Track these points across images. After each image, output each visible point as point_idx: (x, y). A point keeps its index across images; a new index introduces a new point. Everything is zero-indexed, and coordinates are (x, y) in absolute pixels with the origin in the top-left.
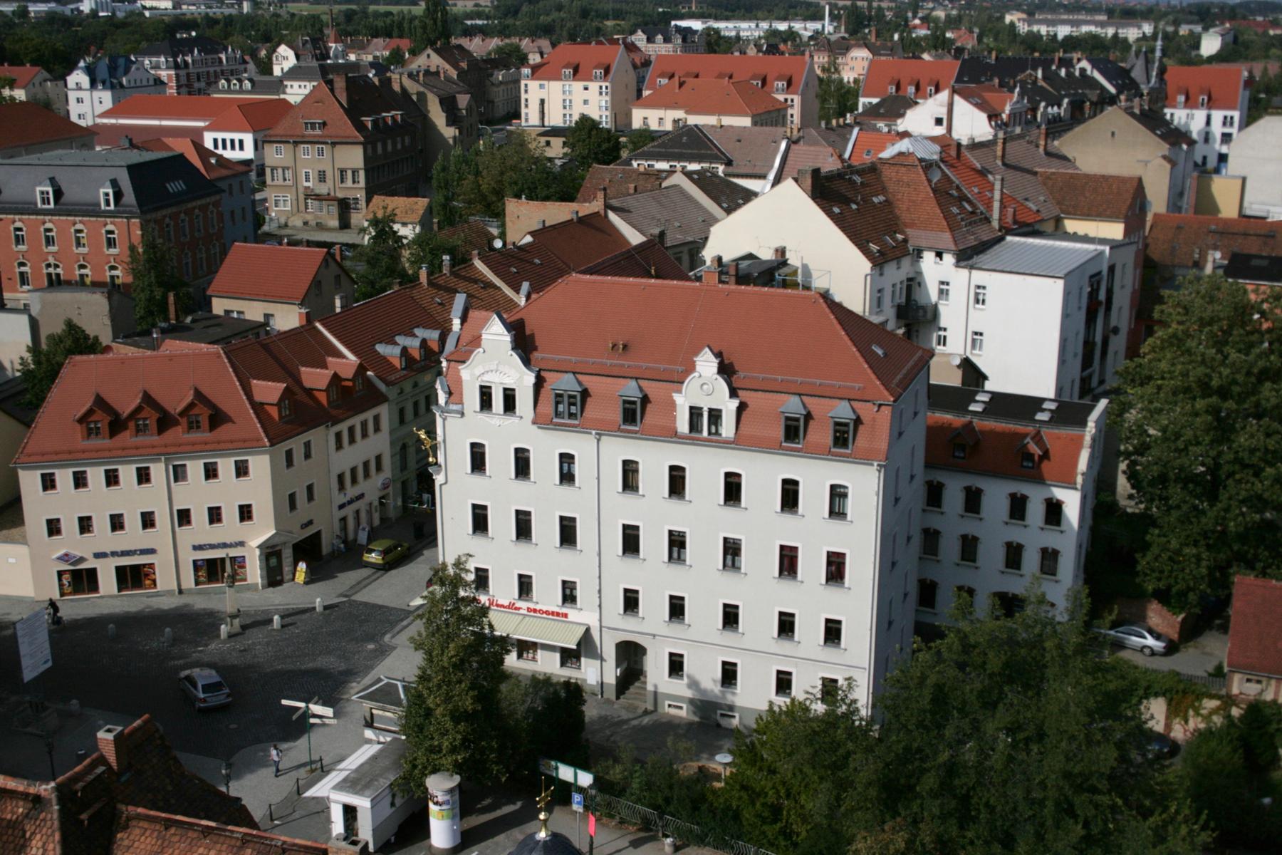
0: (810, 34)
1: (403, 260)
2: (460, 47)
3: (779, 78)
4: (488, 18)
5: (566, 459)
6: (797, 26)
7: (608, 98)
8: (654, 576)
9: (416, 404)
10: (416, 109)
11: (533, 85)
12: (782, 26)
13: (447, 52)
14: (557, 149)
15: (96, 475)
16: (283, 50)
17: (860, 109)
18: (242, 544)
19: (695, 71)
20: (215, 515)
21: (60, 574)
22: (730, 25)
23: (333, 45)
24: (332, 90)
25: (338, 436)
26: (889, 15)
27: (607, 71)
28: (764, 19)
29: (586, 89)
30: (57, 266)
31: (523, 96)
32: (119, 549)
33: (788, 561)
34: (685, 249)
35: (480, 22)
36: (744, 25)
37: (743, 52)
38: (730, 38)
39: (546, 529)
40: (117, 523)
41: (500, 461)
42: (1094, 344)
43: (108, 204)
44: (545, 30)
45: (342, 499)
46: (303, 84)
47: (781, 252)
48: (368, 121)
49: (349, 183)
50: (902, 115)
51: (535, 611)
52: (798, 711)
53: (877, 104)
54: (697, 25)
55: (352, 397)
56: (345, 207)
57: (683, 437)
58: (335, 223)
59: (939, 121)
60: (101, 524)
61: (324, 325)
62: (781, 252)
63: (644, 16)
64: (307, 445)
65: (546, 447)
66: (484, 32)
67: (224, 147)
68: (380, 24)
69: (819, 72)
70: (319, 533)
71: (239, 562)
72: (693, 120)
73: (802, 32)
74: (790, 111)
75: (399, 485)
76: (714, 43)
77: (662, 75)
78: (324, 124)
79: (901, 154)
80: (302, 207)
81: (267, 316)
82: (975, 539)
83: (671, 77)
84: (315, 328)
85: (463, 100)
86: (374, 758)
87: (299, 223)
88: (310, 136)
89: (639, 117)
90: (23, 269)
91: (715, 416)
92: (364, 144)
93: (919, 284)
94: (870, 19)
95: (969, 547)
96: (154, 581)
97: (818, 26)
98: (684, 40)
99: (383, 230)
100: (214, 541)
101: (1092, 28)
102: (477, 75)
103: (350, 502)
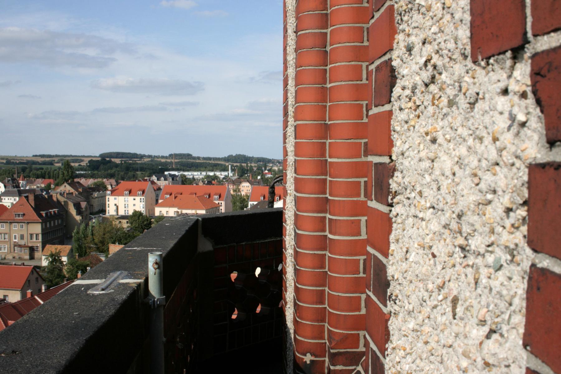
0: (223, 177)
1: (64, 271)
2: (78, 183)
3: (216, 194)
4: (85, 171)
6: (218, 174)
7: (144, 203)
10: (63, 208)
11: (112, 198)
12: (211, 174)
13: (72, 185)
14: (125, 224)
17: (249, 207)
19: (195, 192)
22: (190, 173)
23: (21, 182)
24: (28, 200)
26: (255, 169)
27: (143, 192)
28: (203, 171)
29: (134, 199)
31: (107, 203)
35: (82, 172)
36: (195, 173)
37: (197, 184)
38: (190, 179)
44: (111, 176)
46: (10, 198)
48: (43, 213)
49: (34, 240)
53: (256, 204)
54: (176, 173)
56: (32, 250)
58: (27, 257)
61: (39, 297)
63: (153, 170)
66: (85, 176)
68: (39, 172)
69: (232, 192)
72: (184, 211)
73: (220, 176)
74: (221, 208)
76: (185, 181)
77: (167, 194)
78: (24, 215)
80: (12, 250)
81: (5, 296)
83: (171, 194)
84: (35, 298)
85: (84, 205)
87: (11, 257)
88: (17, 220)
89: (158, 211)
92: (42, 223)
94: (247, 171)
97: (226, 173)
98: (173, 179)
99: (55, 258)
102: (87, 192)
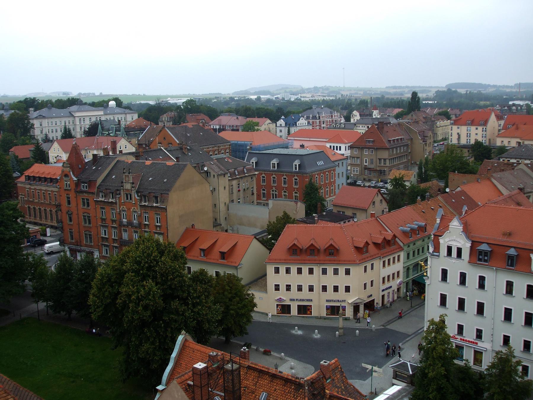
5: (482, 279)
9: (414, 252)
15: (294, 269)
16: (355, 113)
18: (344, 301)
20: (336, 289)
25: (384, 262)
29: (477, 129)
30: (276, 191)
32: (299, 298)
39: (471, 307)
40: (300, 288)
41: (454, 277)
51: (464, 340)
55: (386, 246)
60: (294, 288)
64: (372, 265)
65: (473, 274)
70: (374, 300)
71: (344, 308)
75: (405, 284)
86: (399, 391)
96: (311, 312)
100: (334, 299)
103: (386, 289)
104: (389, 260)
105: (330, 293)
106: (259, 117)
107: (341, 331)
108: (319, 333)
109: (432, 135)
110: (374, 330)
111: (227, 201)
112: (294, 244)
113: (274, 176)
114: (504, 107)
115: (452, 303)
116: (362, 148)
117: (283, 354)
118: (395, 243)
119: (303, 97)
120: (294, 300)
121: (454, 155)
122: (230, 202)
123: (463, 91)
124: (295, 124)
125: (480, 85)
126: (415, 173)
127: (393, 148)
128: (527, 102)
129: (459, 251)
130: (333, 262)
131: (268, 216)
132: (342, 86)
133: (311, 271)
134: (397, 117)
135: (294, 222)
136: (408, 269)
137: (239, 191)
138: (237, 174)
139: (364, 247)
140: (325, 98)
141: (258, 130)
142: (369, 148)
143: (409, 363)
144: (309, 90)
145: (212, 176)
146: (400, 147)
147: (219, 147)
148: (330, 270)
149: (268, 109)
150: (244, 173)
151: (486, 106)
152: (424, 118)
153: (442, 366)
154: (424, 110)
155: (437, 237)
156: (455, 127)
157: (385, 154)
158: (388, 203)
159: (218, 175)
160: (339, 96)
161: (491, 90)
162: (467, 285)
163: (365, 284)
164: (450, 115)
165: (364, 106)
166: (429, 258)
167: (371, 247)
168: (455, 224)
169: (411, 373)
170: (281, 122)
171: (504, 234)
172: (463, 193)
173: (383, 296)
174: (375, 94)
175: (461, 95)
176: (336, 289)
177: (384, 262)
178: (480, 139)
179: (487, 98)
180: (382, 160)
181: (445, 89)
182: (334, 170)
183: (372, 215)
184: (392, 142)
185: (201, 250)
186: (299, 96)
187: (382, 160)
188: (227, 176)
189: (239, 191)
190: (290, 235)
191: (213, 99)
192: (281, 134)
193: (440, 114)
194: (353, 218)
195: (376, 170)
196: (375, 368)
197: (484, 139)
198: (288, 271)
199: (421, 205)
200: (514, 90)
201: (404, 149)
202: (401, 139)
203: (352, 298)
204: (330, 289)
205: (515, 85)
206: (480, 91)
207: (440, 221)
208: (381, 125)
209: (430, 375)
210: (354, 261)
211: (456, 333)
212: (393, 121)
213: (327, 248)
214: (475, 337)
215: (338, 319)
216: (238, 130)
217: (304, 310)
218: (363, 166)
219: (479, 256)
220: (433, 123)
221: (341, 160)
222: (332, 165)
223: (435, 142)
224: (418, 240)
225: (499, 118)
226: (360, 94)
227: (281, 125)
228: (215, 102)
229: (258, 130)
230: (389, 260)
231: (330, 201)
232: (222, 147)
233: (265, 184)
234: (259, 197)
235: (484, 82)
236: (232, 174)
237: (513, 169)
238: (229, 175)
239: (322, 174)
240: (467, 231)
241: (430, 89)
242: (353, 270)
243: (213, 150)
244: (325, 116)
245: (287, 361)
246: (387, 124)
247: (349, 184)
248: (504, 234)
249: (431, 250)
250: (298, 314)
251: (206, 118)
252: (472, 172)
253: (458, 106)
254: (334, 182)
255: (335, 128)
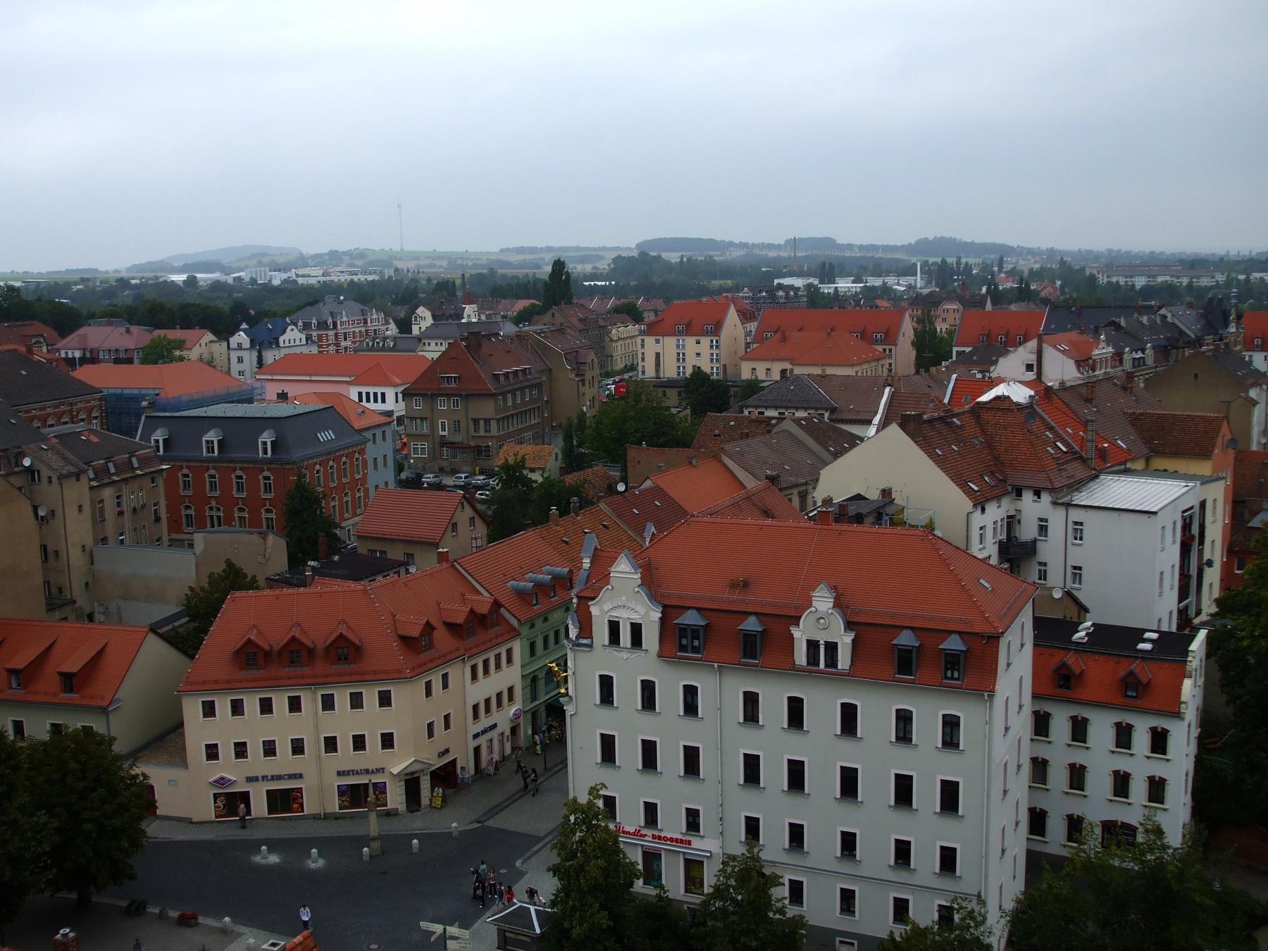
5: (690, 692)
8: (774, 807)
9: (546, 639)
15: (252, 703)
16: (422, 311)
20: (359, 742)
21: (216, 796)
25: (474, 668)
29: (698, 343)
30: (219, 510)
33: (904, 789)
34: (795, 491)
39: (671, 760)
41: (628, 694)
42: (1189, 577)
43: (265, 452)
45: (479, 727)
47: (886, 493)
50: (995, 363)
51: (659, 838)
52: (919, 933)
55: (477, 630)
57: (802, 669)
59: (1029, 367)
62: (886, 493)
64: (445, 677)
67: (368, 400)
70: (454, 761)
71: (381, 788)
75: (529, 716)
79: (998, 398)
82: (1083, 768)
90: (188, 512)
91: (832, 648)
93: (1019, 522)
95: (1077, 776)
97: (910, 280)
101: (1168, 278)
103: (484, 732)
104: (486, 663)
105: (346, 755)
106: (187, 325)
107: (376, 844)
108: (320, 855)
109: (596, 361)
110: (455, 834)
111: (89, 542)
112: (249, 641)
113: (212, 472)
114: (760, 292)
115: (629, 754)
116: (431, 396)
117: (227, 919)
118: (501, 620)
119: (303, 276)
120: (256, 779)
121: (641, 405)
122: (96, 543)
123: (673, 257)
124: (274, 343)
125: (711, 243)
126: (556, 450)
127: (504, 394)
128: (811, 280)
129: (636, 630)
130: (430, 665)
131: (193, 574)
132: (396, 248)
133: (295, 705)
134: (518, 320)
135: (253, 585)
136: (534, 680)
137: (121, 513)
138: (113, 471)
139: (422, 635)
140: (355, 278)
141: (181, 359)
142: (449, 396)
143: (532, 908)
144: (318, 259)
145: (45, 480)
146: (522, 389)
147: (71, 404)
148: (342, 698)
149: (208, 307)
150: (134, 469)
151: (721, 290)
152: (580, 320)
153: (602, 907)
154: (582, 301)
155: (585, 600)
156: (650, 340)
157: (486, 409)
158: (488, 524)
159: (62, 478)
160: (388, 272)
161: (736, 254)
162: (657, 710)
163: (430, 726)
164: (641, 313)
165: (444, 294)
166: (569, 652)
167: (441, 635)
168: (624, 570)
169: (538, 931)
170: (241, 338)
171: (734, 585)
172: (657, 491)
173: (477, 750)
174: (475, 266)
175: (669, 267)
176: (359, 742)
177: (474, 668)
178: (706, 368)
179: (726, 271)
180: (482, 422)
181: (635, 254)
182: (362, 452)
183: (443, 557)
184: (502, 378)
185: (11, 672)
186: (292, 274)
187: (482, 422)
188: (84, 479)
189: (121, 513)
190: (240, 618)
191: (76, 284)
192: (241, 367)
193: (617, 310)
194: (405, 564)
195: (470, 447)
196: (453, 930)
197: (715, 365)
198: (237, 708)
199: (559, 527)
200: (786, 255)
201: (531, 395)
202: (524, 371)
203: (398, 763)
204: (345, 744)
205: (788, 242)
206: (711, 257)
207: (591, 563)
208: (475, 340)
209: (577, 932)
210: (400, 672)
211: (642, 823)
212: (508, 329)
213: (331, 644)
214: (684, 830)
215: (364, 816)
216: (130, 361)
217: (284, 801)
218: (438, 439)
219: (682, 641)
220: (603, 331)
221: (379, 426)
222: (354, 438)
223: (608, 375)
224: (553, 610)
225: (746, 316)
226: (440, 267)
227: (240, 347)
228: (79, 291)
229: (181, 359)
230: (486, 663)
231: (350, 527)
232: (80, 405)
233: (190, 493)
234: (175, 526)
235: (719, 237)
236: (101, 473)
237: (769, 432)
238: (92, 476)
239: (331, 463)
240: (651, 583)
241: (601, 253)
242: (398, 694)
243: (54, 414)
244: (348, 321)
245: (240, 935)
246: (488, 337)
247: (403, 484)
248: (734, 585)
249: (573, 633)
250: (270, 812)
251: (48, 332)
252: (682, 442)
253: (649, 290)
254: (364, 480)
255: (372, 349)
